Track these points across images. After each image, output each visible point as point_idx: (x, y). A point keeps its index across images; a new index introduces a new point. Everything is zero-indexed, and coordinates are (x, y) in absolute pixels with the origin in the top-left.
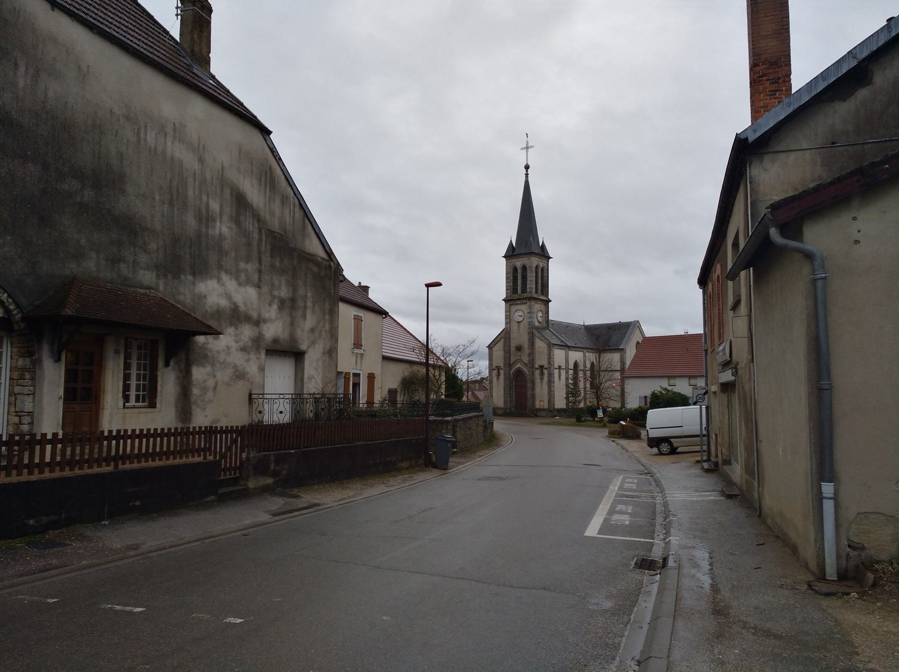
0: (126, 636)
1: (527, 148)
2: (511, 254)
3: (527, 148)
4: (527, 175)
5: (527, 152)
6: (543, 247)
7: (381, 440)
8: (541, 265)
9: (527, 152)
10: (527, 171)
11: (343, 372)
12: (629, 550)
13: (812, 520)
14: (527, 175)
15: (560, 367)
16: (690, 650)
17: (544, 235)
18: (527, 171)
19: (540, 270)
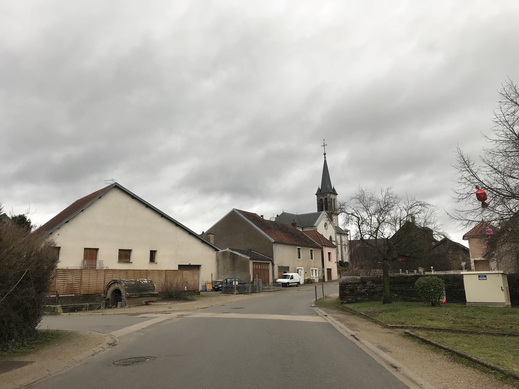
0: (435, 298)
1: (324, 145)
2: (320, 193)
3: (324, 145)
4: (325, 157)
5: (324, 147)
6: (334, 190)
7: (51, 307)
8: (333, 198)
9: (324, 147)
10: (325, 156)
11: (290, 279)
12: (514, 260)
13: (471, 229)
14: (325, 157)
15: (345, 245)
16: (429, 294)
17: (334, 183)
18: (325, 156)
19: (333, 200)
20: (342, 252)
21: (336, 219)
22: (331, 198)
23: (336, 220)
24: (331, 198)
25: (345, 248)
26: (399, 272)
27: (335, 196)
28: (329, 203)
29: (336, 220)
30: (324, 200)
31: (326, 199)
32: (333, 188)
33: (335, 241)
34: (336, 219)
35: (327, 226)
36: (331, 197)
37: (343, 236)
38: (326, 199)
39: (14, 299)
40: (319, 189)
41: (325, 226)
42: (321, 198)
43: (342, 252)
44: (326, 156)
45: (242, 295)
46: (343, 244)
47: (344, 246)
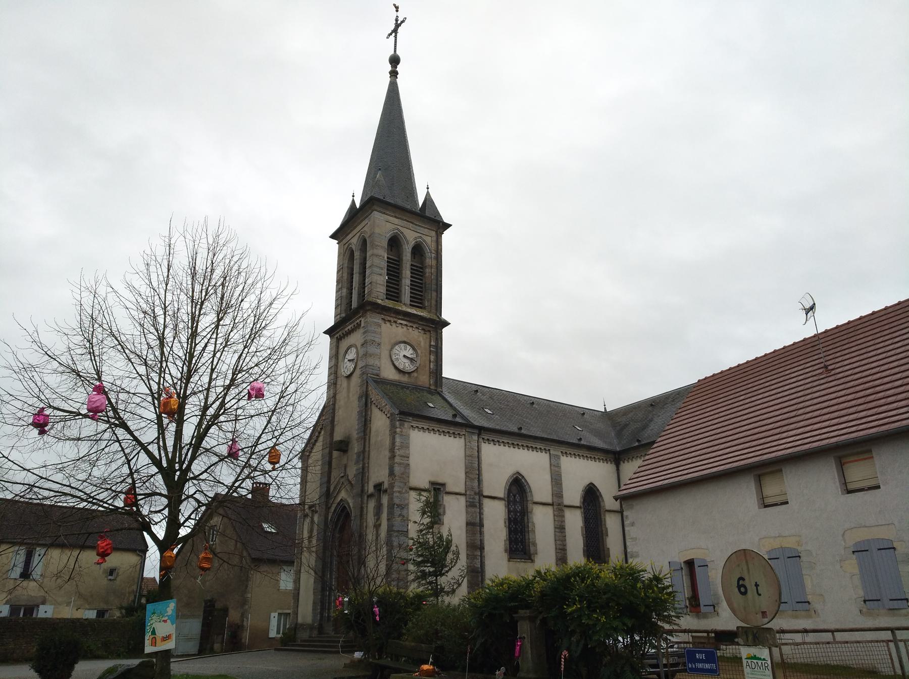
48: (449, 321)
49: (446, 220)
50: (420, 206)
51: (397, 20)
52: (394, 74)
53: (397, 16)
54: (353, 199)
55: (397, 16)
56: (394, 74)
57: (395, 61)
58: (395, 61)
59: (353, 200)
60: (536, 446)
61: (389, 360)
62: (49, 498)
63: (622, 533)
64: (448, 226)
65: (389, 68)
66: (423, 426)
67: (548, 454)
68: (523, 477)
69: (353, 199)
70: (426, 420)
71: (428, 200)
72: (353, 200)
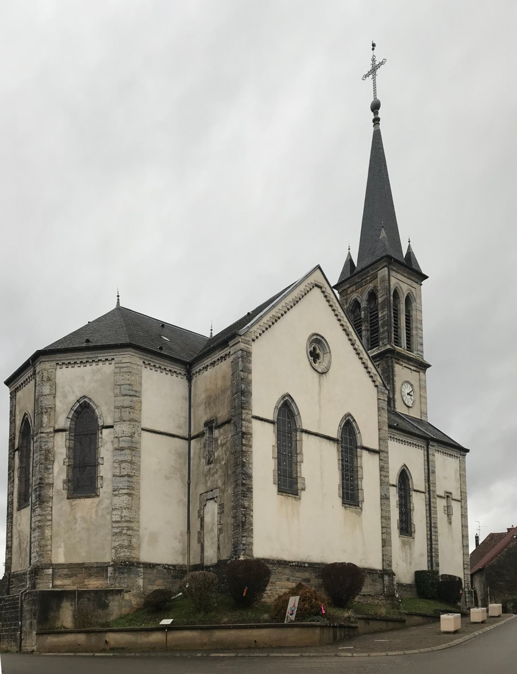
9: (374, 78)
20: (431, 527)
21: (416, 384)
22: (396, 292)
23: (416, 388)
24: (396, 292)
25: (449, 515)
26: (19, 606)
27: (415, 285)
28: (383, 308)
29: (416, 388)
30: (364, 305)
31: (373, 296)
32: (404, 253)
33: (376, 447)
34: (416, 384)
35: (327, 357)
36: (393, 281)
37: (437, 455)
38: (373, 296)
39: (308, 602)
40: (350, 261)
41: (314, 356)
42: (354, 296)
43: (431, 527)
44: (379, 116)
45: (13, 519)
46: (440, 492)
47: (440, 504)
48: (430, 364)
49: (424, 272)
50: (404, 256)
51: (373, 60)
52: (376, 121)
53: (374, 56)
54: (349, 251)
55: (374, 56)
56: (376, 121)
57: (375, 107)
58: (375, 107)
59: (349, 254)
60: (413, 442)
61: (404, 406)
62: (112, 500)
63: (187, 526)
64: (426, 277)
65: (372, 116)
66: (106, 358)
67: (458, 460)
68: (412, 478)
69: (349, 251)
70: (110, 349)
71: (410, 253)
72: (349, 254)
